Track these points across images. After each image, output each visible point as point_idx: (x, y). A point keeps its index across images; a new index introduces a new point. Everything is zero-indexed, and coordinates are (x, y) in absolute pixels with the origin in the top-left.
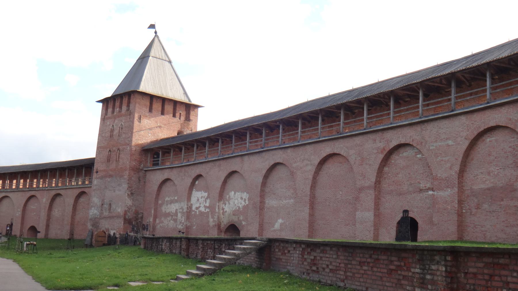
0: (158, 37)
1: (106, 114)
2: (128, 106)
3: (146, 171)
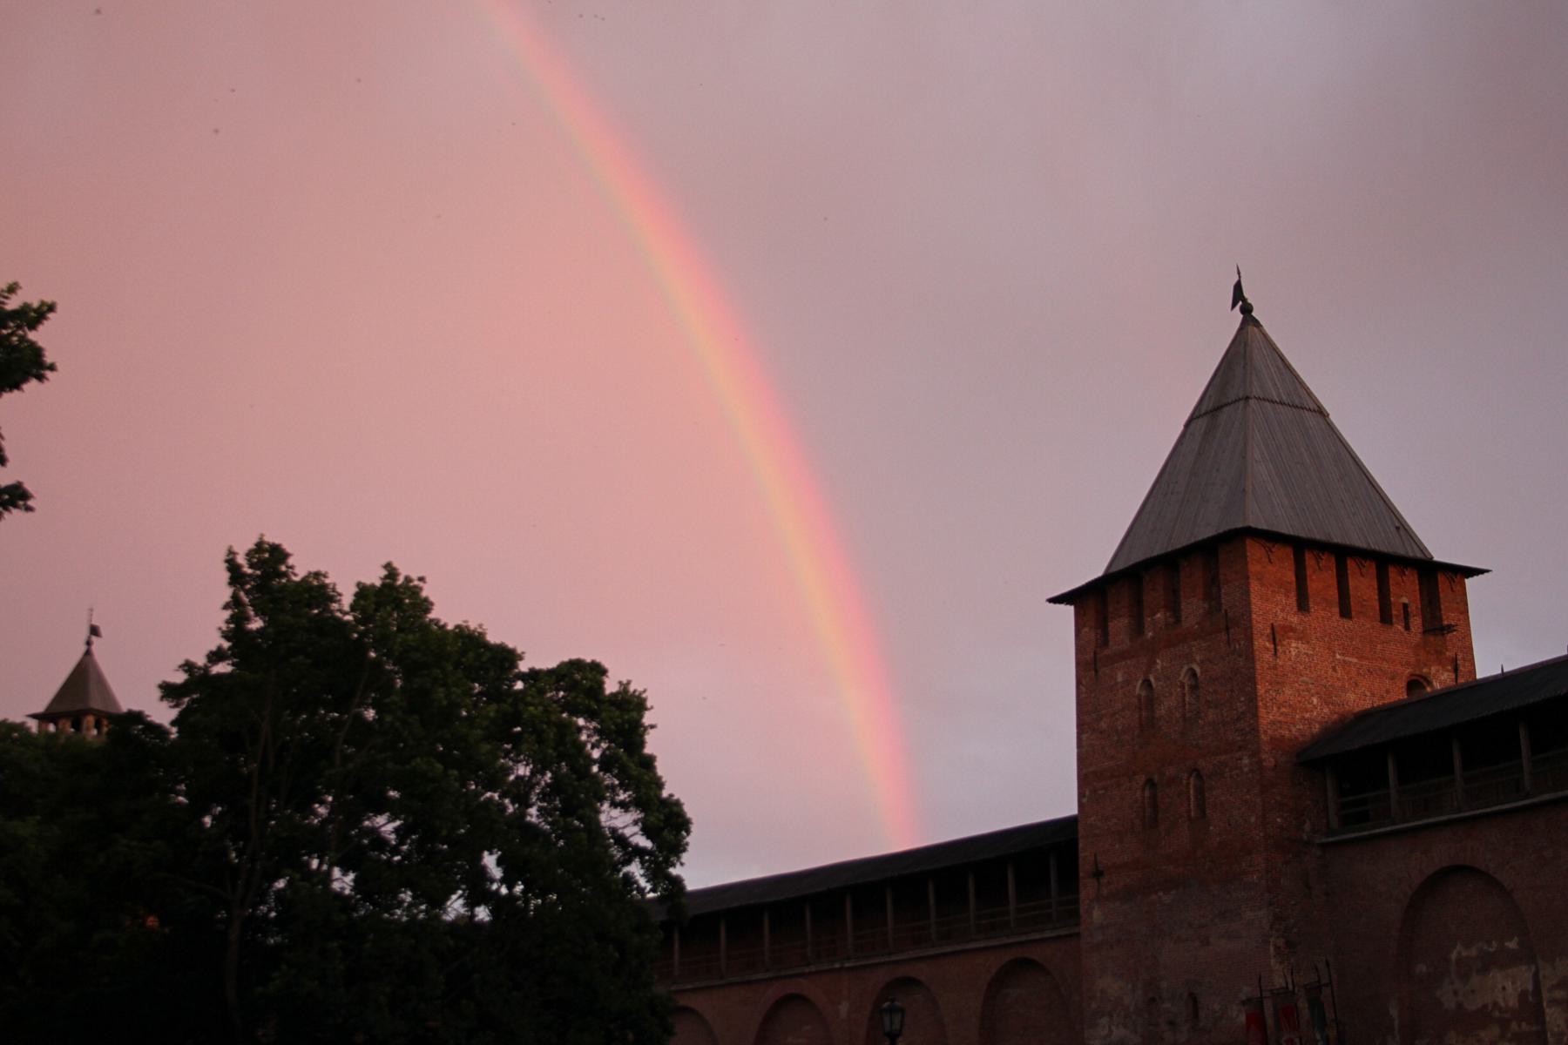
0: (1256, 323)
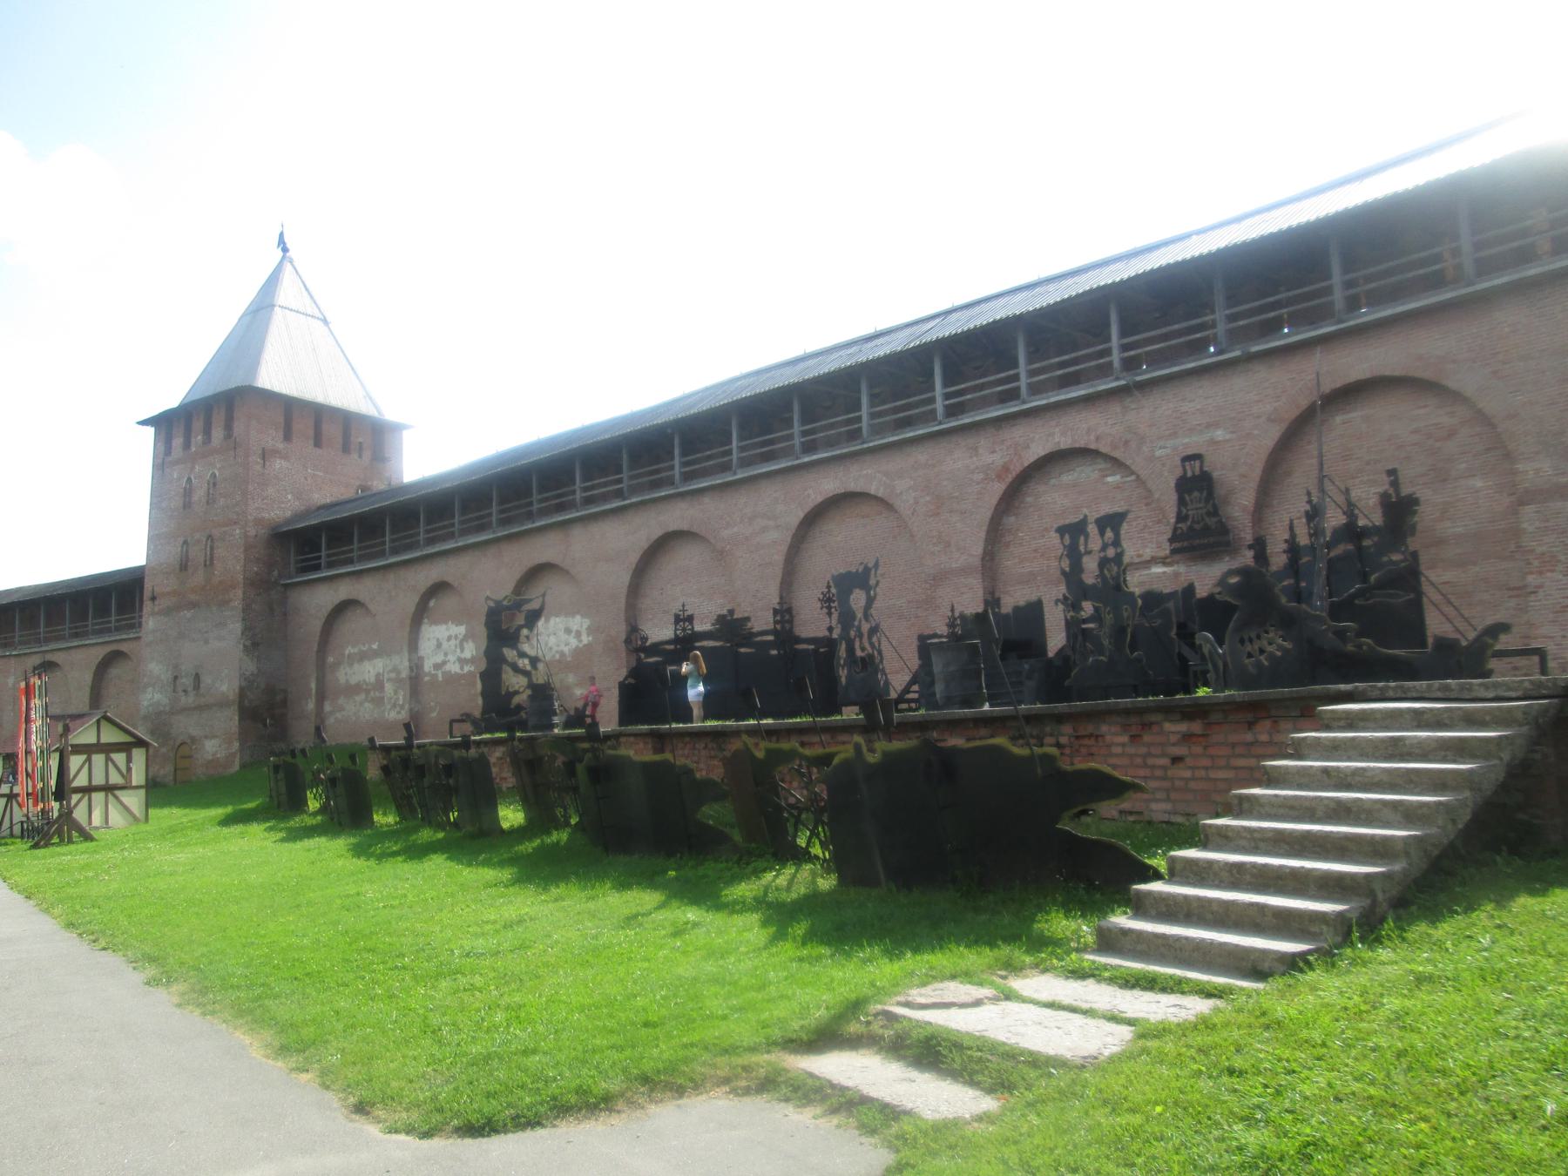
0: (291, 262)
1: (168, 452)
2: (228, 427)
3: (286, 586)
